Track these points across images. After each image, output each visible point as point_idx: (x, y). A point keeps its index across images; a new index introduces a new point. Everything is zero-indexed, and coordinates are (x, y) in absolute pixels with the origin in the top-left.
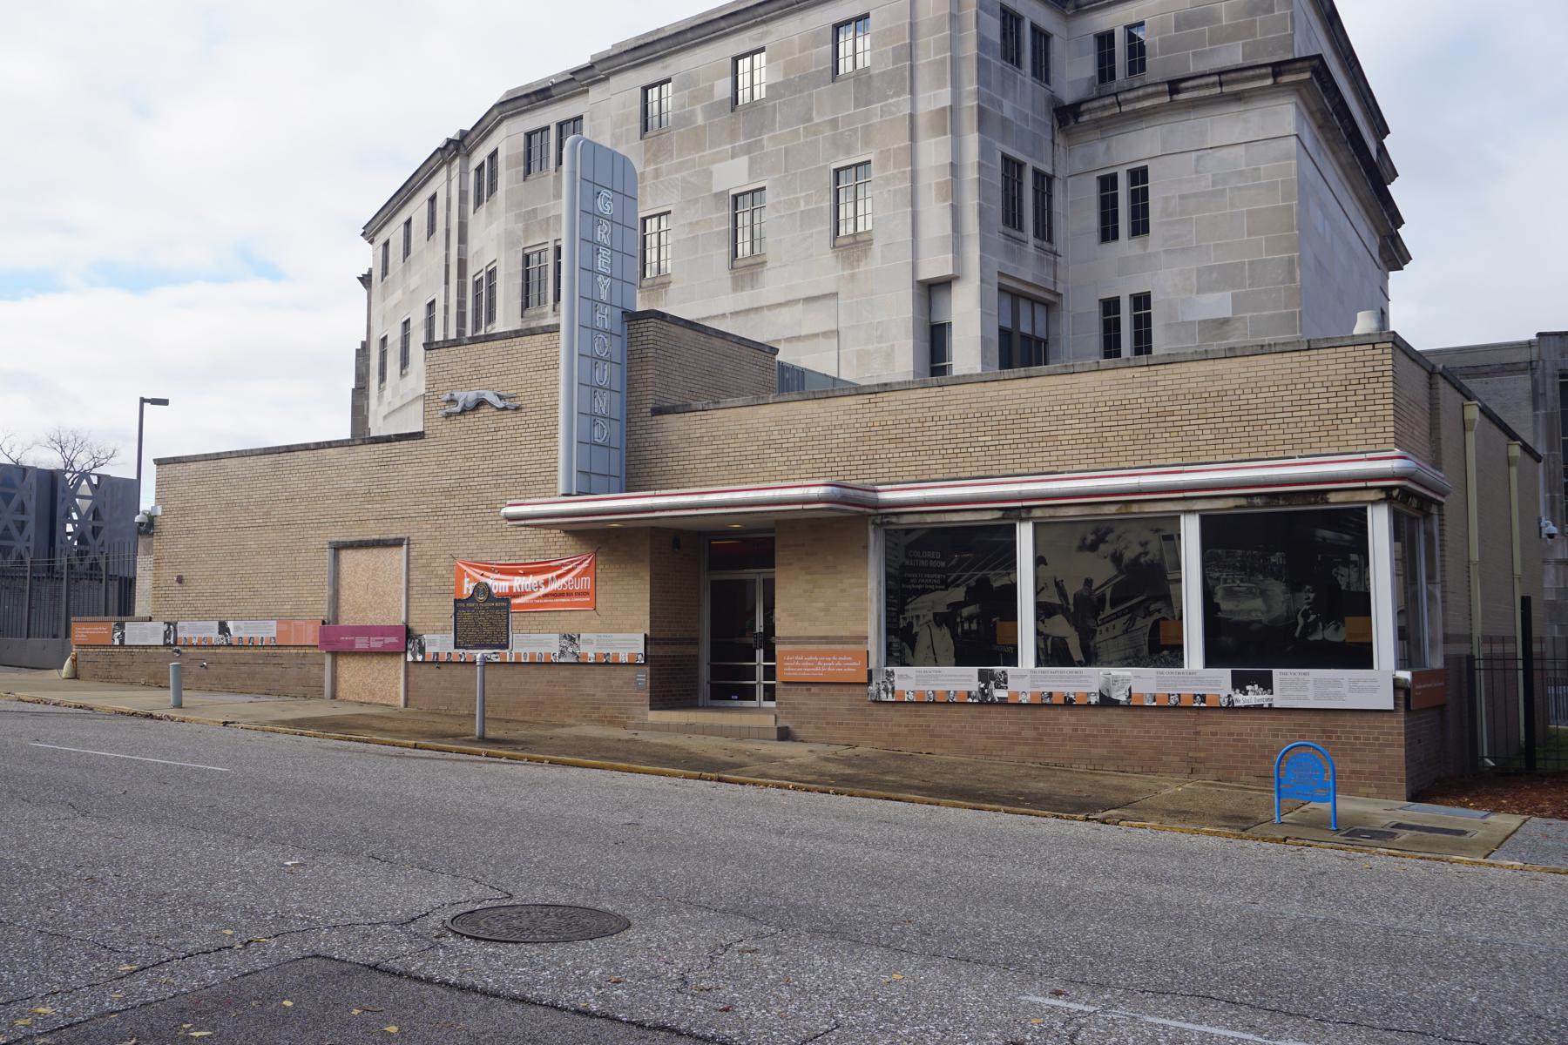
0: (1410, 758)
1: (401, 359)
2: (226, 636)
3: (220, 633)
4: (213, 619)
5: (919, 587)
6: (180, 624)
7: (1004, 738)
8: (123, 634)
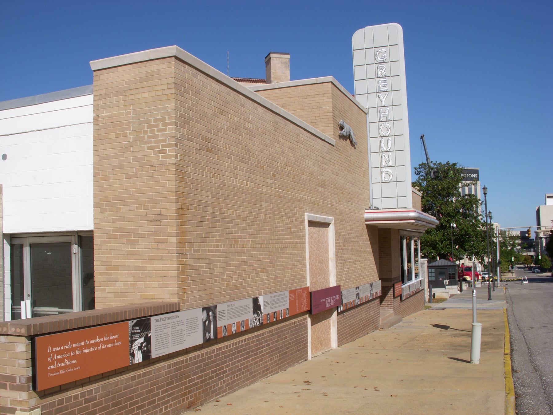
0: (43, 399)
1: (264, 108)
2: (258, 315)
3: (254, 313)
4: (244, 297)
5: (135, 339)
6: (219, 309)
7: (272, 335)
8: (148, 340)
